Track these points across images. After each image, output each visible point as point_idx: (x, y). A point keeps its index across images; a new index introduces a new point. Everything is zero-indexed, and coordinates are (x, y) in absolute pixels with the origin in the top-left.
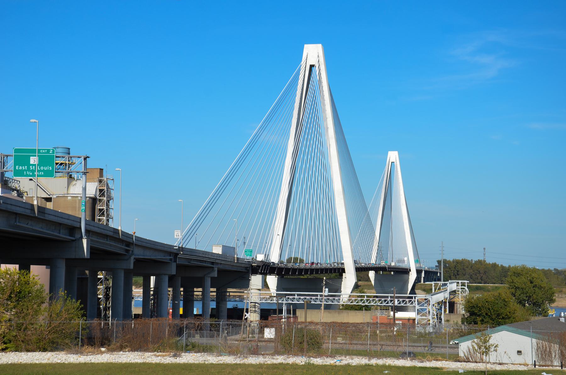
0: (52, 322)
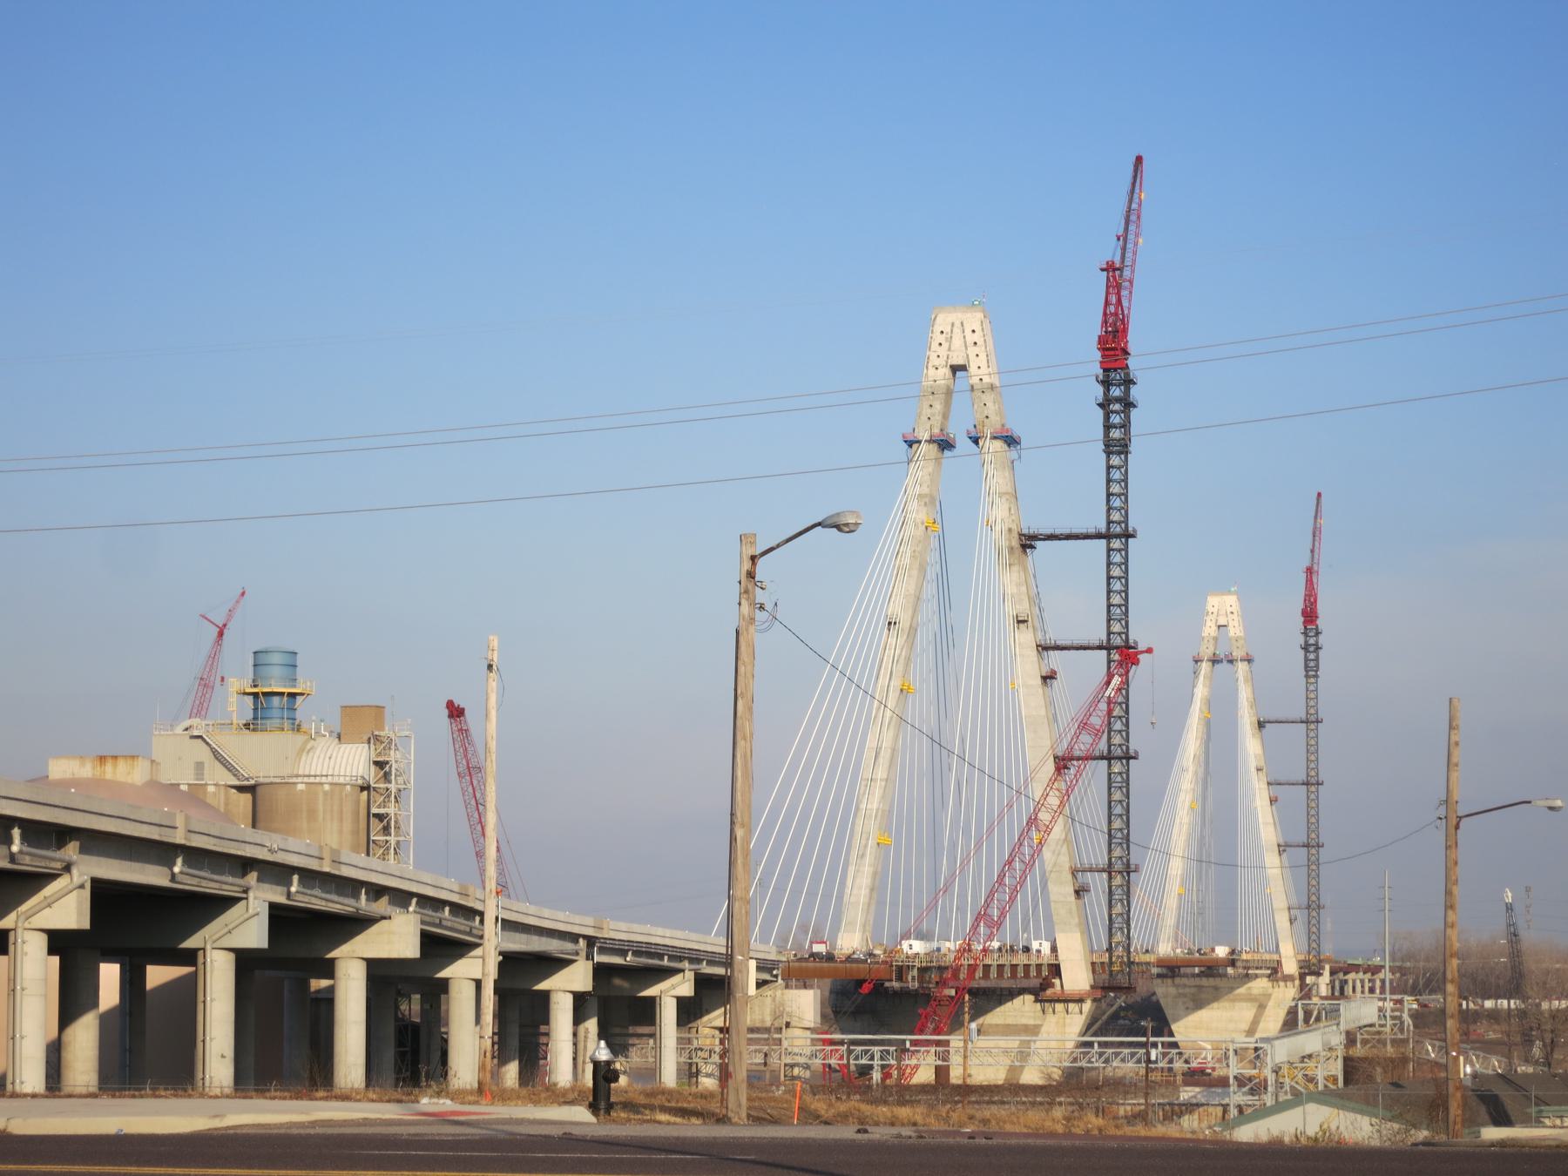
0: (890, 1099)
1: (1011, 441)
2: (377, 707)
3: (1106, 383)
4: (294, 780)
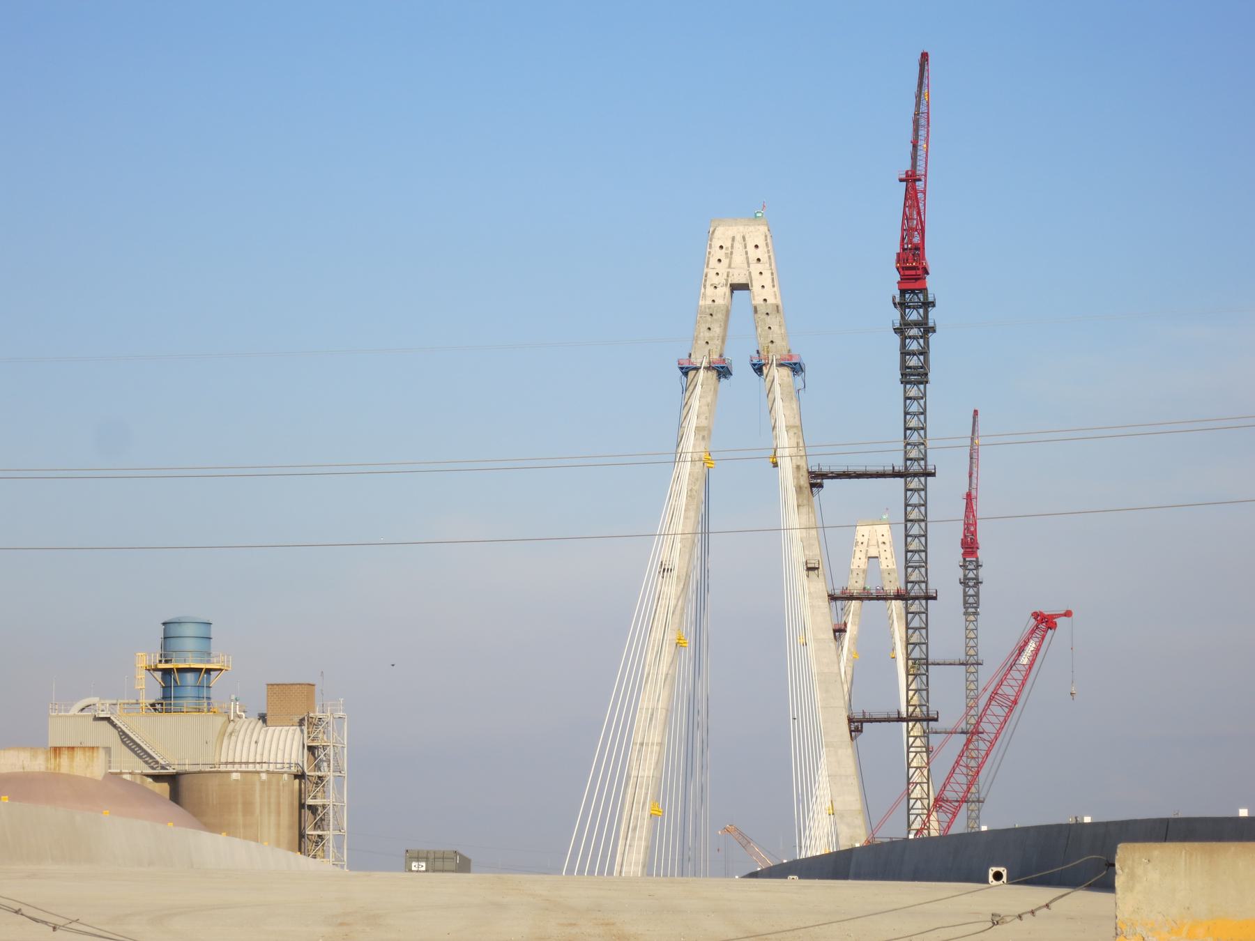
1: (796, 368)
2: (309, 685)
3: (902, 305)
4: (229, 768)
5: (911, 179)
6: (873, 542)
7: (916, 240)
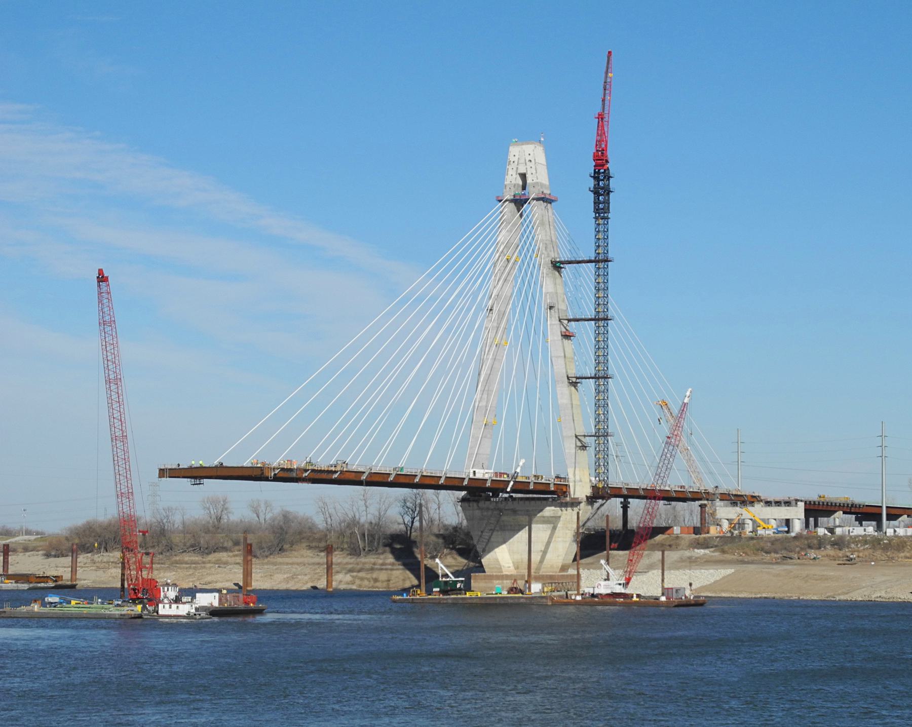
5: (601, 117)
6: (522, 161)
7: (603, 146)
